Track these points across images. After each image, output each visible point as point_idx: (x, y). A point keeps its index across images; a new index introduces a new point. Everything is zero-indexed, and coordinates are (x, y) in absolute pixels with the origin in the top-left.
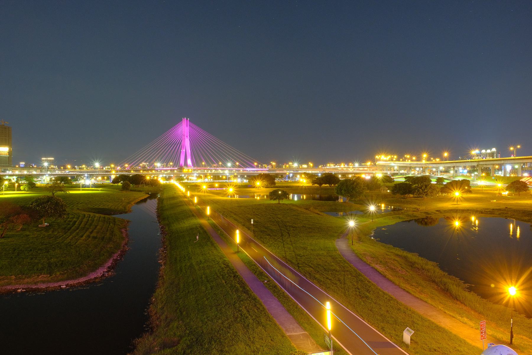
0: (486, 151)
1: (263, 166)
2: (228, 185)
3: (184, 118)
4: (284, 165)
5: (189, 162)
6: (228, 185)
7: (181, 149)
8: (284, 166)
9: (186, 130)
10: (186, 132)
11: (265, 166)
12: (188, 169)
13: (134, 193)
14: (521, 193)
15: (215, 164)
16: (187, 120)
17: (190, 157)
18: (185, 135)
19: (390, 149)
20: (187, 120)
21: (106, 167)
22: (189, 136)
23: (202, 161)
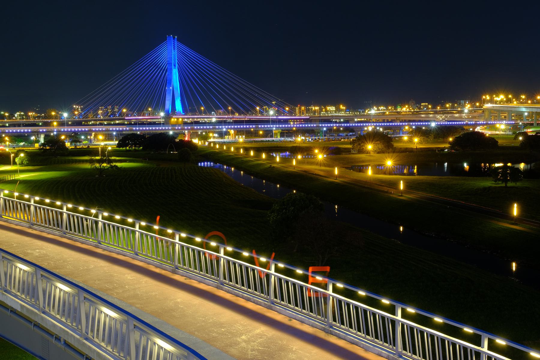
0: (516, 184)
1: (263, 109)
2: (243, 143)
3: (169, 35)
4: (297, 106)
5: (179, 107)
6: (243, 143)
7: (165, 87)
8: (297, 108)
9: (173, 56)
10: (173, 58)
11: (266, 108)
12: (178, 119)
13: (355, 155)
14: (416, 147)
15: (222, 109)
16: (174, 38)
17: (180, 98)
18: (171, 63)
19: (506, 90)
20: (174, 38)
21: (18, 113)
22: (177, 65)
23: (199, 106)
